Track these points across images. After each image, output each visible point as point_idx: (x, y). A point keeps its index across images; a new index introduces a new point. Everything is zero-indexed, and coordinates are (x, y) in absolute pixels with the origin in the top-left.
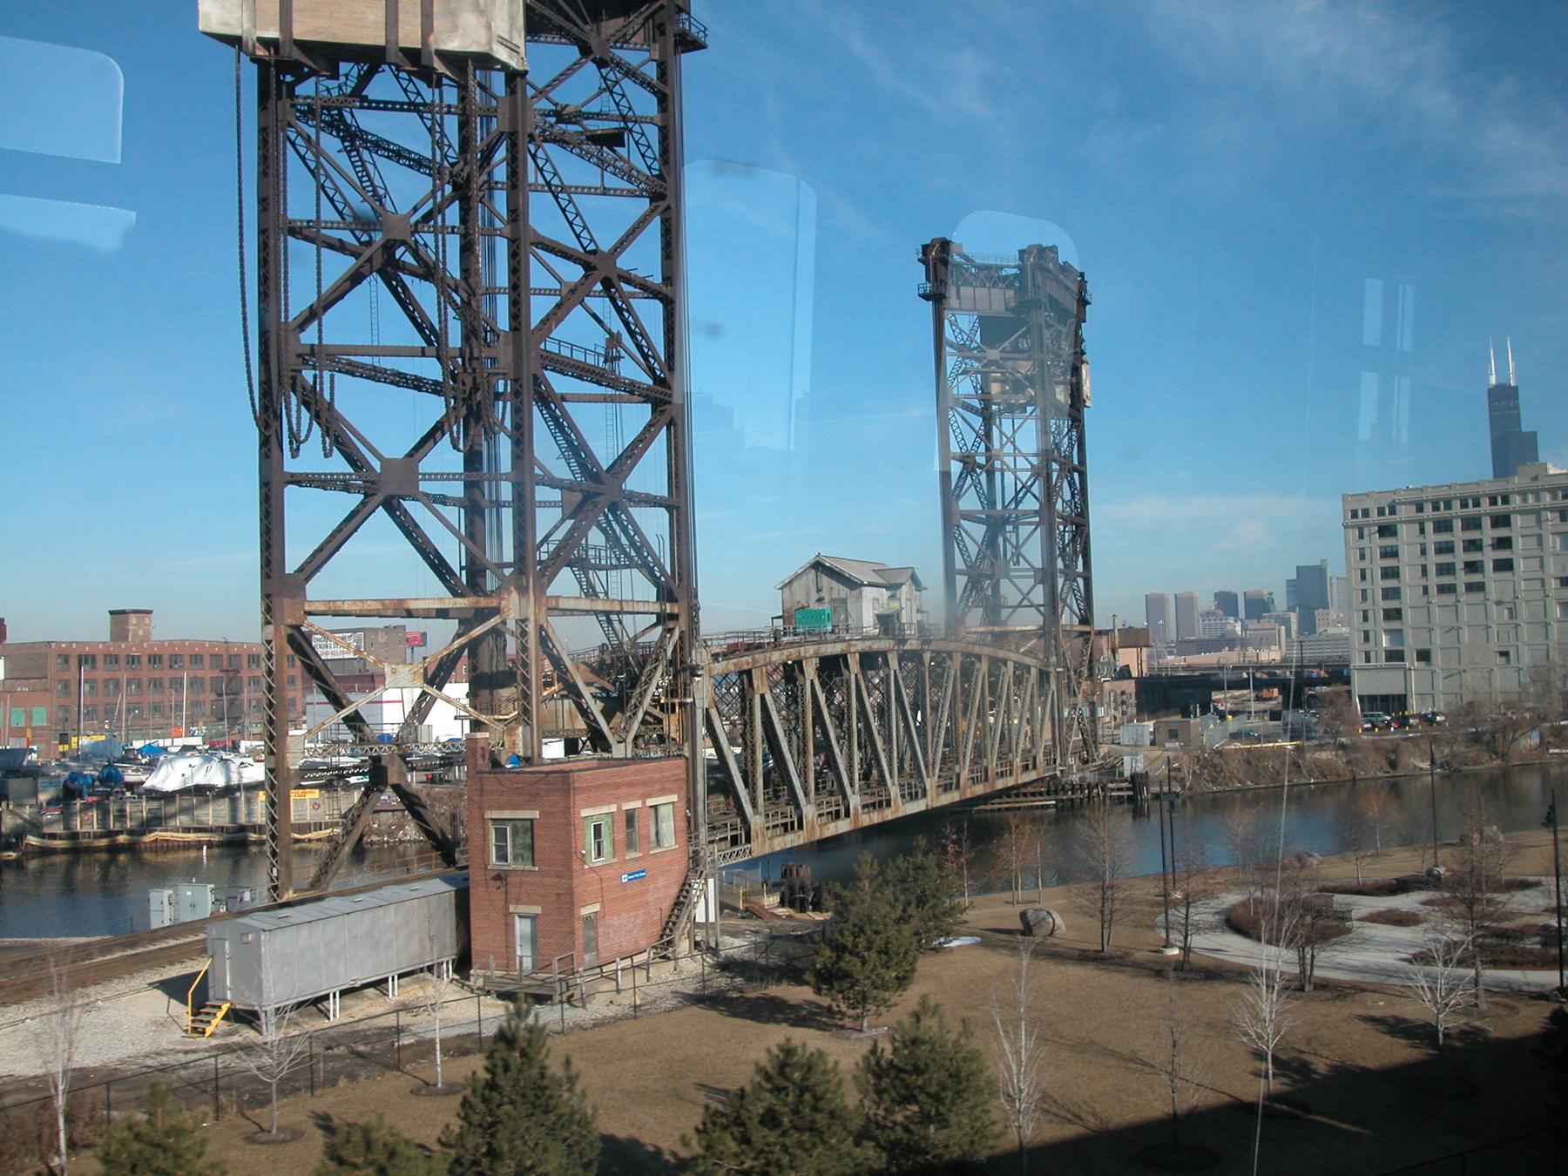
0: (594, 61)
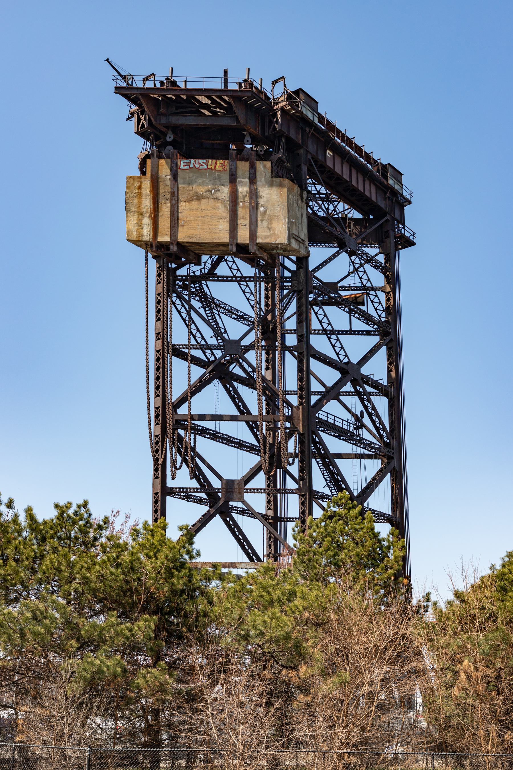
0: (347, 252)
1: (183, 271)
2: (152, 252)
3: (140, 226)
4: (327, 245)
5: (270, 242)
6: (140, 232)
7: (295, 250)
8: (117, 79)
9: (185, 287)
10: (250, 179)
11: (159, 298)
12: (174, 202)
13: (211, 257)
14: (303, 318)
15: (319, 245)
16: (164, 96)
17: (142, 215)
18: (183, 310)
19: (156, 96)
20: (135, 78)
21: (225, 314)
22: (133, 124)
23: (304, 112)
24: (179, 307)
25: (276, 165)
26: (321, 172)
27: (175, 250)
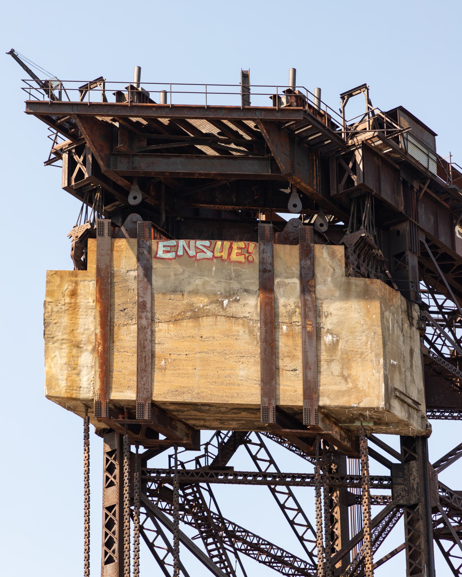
1: (159, 462)
2: (99, 421)
3: (75, 369)
4: (456, 414)
5: (347, 405)
6: (73, 381)
7: (399, 422)
8: (31, 87)
9: (167, 496)
10: (302, 278)
11: (110, 515)
12: (144, 322)
13: (218, 434)
14: (420, 563)
15: (438, 414)
16: (125, 119)
17: (78, 347)
18: (160, 542)
19: (108, 119)
20: (66, 85)
21: (245, 552)
22: (59, 173)
23: (409, 152)
24: (151, 536)
25: (354, 252)
26: (445, 269)
27: (146, 417)
